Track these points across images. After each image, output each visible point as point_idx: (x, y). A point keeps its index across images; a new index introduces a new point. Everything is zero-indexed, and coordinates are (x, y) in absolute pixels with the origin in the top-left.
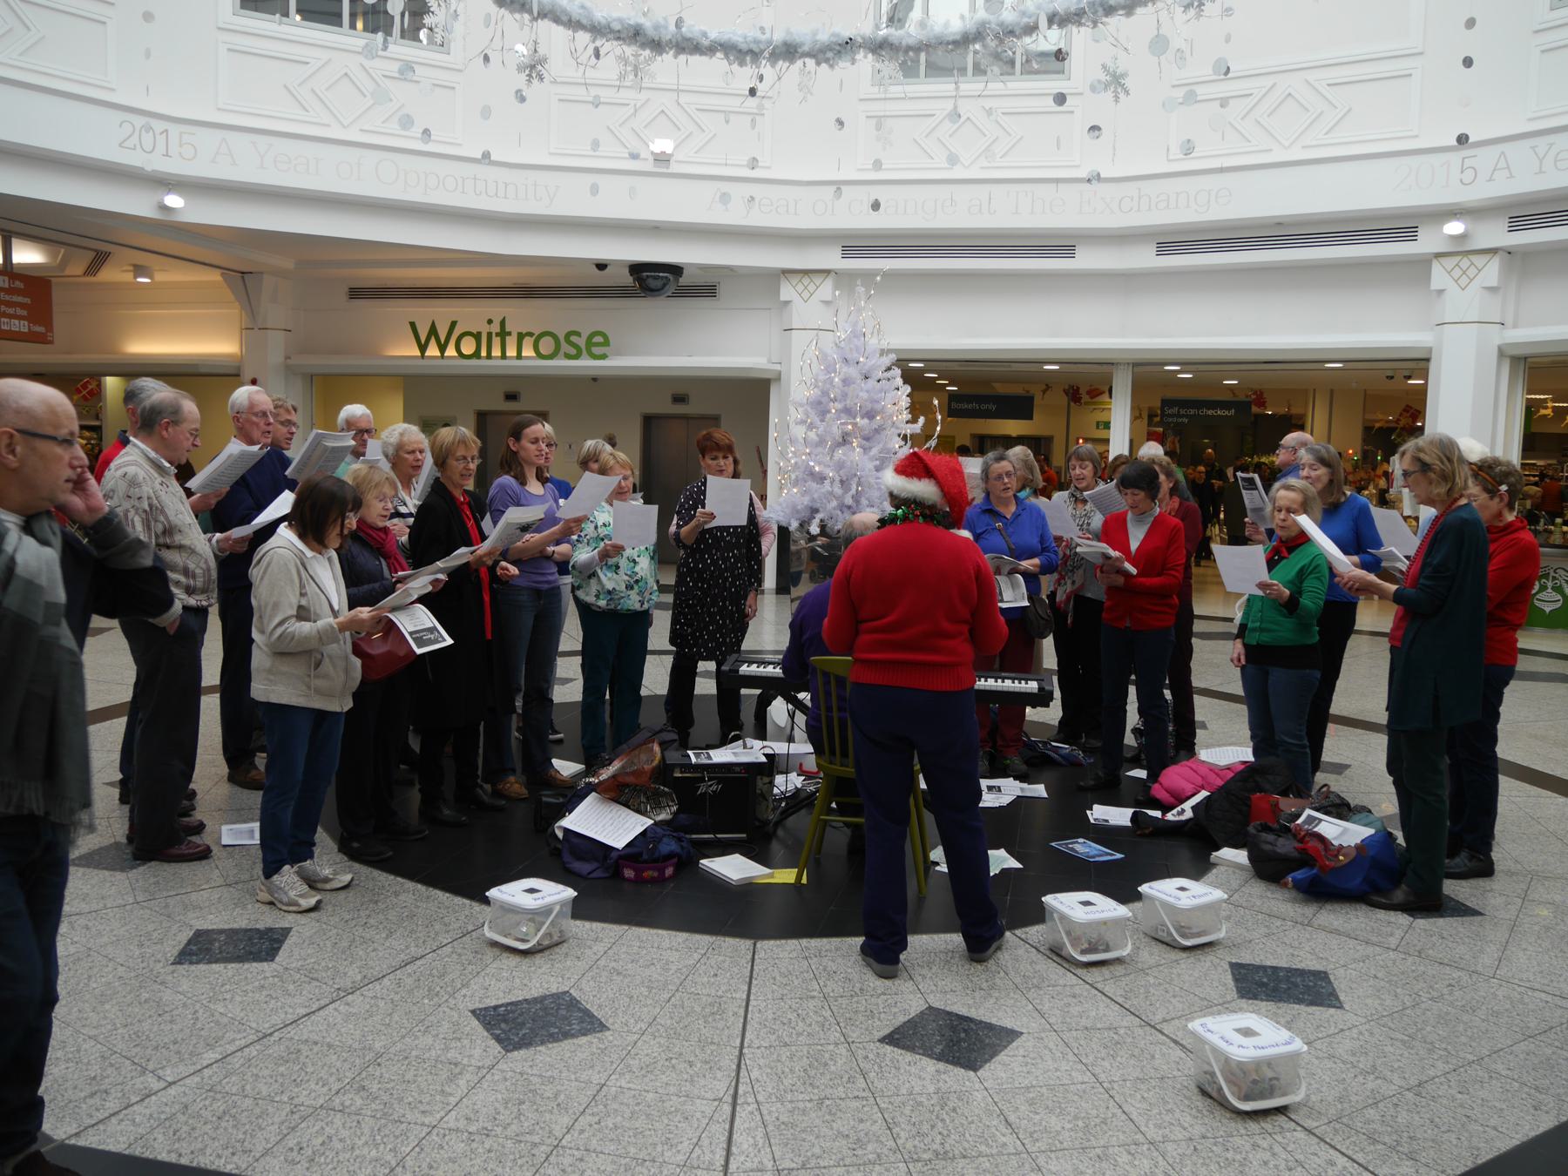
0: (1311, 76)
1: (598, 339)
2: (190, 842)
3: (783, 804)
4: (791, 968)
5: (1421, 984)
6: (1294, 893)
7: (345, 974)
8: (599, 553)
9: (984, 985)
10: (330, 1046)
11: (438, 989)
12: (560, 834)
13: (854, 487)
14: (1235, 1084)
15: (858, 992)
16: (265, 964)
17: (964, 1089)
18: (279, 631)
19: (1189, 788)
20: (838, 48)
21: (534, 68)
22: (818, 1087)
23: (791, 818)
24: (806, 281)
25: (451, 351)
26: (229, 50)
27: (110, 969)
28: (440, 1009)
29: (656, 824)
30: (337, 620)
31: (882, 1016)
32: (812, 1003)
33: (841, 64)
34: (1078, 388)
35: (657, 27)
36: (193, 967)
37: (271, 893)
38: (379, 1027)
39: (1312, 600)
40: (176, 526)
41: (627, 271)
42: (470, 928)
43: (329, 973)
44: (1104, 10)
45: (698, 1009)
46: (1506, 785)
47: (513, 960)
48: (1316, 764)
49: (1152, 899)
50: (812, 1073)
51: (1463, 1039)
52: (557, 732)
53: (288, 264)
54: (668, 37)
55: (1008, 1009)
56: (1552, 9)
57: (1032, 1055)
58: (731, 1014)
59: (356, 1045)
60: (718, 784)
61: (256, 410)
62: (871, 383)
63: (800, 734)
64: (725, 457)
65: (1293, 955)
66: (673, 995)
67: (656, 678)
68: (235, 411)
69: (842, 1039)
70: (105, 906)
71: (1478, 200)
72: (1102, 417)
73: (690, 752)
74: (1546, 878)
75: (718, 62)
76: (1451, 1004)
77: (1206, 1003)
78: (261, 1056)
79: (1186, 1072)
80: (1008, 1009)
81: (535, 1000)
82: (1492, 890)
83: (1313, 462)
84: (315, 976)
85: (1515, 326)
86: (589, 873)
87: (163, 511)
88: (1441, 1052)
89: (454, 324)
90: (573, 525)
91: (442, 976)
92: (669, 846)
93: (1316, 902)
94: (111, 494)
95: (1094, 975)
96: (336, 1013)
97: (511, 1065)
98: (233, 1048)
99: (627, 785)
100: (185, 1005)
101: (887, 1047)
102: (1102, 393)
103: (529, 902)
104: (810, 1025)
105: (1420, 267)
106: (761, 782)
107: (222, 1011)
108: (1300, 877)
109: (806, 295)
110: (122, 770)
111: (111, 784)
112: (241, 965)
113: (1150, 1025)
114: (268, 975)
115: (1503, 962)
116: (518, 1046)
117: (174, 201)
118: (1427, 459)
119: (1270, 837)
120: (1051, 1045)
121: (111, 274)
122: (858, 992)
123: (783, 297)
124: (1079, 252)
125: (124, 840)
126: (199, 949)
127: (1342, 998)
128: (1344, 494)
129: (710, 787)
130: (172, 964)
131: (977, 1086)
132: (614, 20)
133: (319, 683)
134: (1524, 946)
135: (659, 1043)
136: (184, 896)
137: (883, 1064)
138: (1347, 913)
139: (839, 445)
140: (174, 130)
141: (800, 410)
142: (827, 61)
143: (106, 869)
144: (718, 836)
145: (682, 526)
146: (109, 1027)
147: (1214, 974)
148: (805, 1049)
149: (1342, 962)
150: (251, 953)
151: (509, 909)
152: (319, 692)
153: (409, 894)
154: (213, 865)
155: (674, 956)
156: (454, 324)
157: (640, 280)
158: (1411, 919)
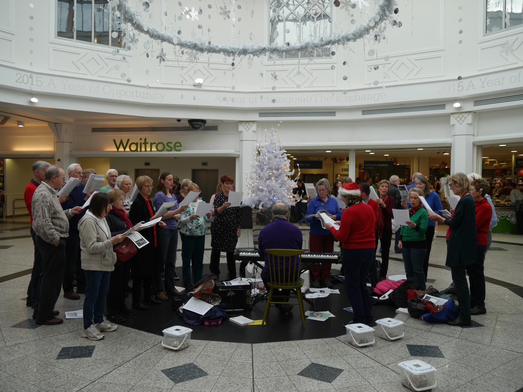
0: (409, 57)
1: (178, 145)
2: (56, 318)
3: (254, 299)
4: (265, 352)
5: (468, 349)
6: (424, 322)
7: (117, 360)
8: (190, 218)
9: (329, 355)
10: (116, 384)
11: (149, 364)
12: (181, 312)
14: (415, 383)
15: (288, 359)
16: (88, 358)
17: (328, 389)
18: (92, 246)
19: (386, 289)
20: (260, 51)
21: (161, 58)
22: (280, 390)
23: (257, 304)
24: (247, 124)
25: (128, 149)
26: (53, 50)
27: (35, 362)
28: (151, 370)
29: (214, 306)
31: (297, 366)
32: (274, 363)
33: (261, 56)
34: (336, 158)
35: (202, 44)
36: (64, 360)
37: (87, 334)
38: (131, 377)
39: (424, 226)
40: (57, 211)
41: (187, 122)
42: (156, 343)
43: (111, 360)
44: (347, 39)
45: (237, 367)
46: (487, 284)
47: (173, 353)
48: (426, 280)
49: (380, 325)
50: (278, 386)
51: (483, 366)
52: (177, 277)
53: (71, 120)
54: (206, 47)
55: (338, 363)
56: (484, 36)
57: (348, 377)
58: (248, 368)
59: (124, 384)
60: (234, 293)
61: (77, 171)
62: (277, 159)
63: (258, 275)
64: (231, 184)
65: (426, 341)
66: (228, 363)
67: (207, 259)
68: (70, 171)
69: (286, 375)
70: (29, 340)
71: (463, 96)
72: (345, 167)
73: (224, 282)
74: (502, 313)
75: (221, 55)
76: (478, 355)
77: (401, 358)
78: (93, 388)
79: (398, 380)
80: (338, 363)
81: (182, 366)
82: (486, 318)
83: (420, 182)
84: (106, 361)
85: (478, 136)
86: (193, 324)
87: (53, 206)
88: (477, 370)
89: (128, 140)
90: (184, 208)
91: (149, 359)
92: (219, 314)
93: (432, 324)
94: (37, 201)
95: (364, 350)
96: (116, 373)
97: (178, 388)
98: (83, 386)
99: (204, 294)
100: (63, 373)
101: (301, 376)
102: (344, 159)
103: (177, 333)
104: (274, 370)
105: (446, 118)
107: (77, 374)
108: (426, 316)
109: (247, 129)
110: (28, 294)
111: (23, 299)
112: (80, 358)
113: (384, 366)
114: (90, 361)
115: (493, 341)
116: (179, 382)
117: (34, 100)
118: (455, 180)
119: (415, 304)
120: (353, 373)
121: (8, 124)
122: (288, 359)
124: (337, 114)
125: (32, 318)
126: (65, 354)
127: (444, 354)
128: (430, 192)
129: (231, 294)
130: (56, 359)
131: (332, 387)
132: (188, 42)
133: (105, 262)
134: (498, 335)
135: (226, 378)
136: (56, 336)
137: (300, 382)
138: (441, 327)
139: (268, 179)
140: (34, 76)
141: (254, 168)
142: (257, 55)
143: (27, 328)
144: (235, 310)
145: (217, 208)
146: (38, 381)
147: (401, 349)
148: (274, 378)
149: (442, 343)
150: (83, 354)
151: (170, 336)
152: (105, 265)
153: (133, 333)
154: (64, 325)
155: (226, 350)
156: (128, 140)
157: (192, 125)
158: (462, 328)
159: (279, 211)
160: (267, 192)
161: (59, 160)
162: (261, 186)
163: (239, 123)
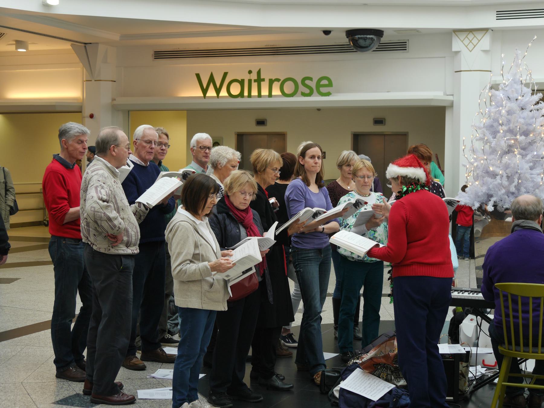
1: (325, 82)
3: (474, 383)
12: (337, 395)
13: (516, 180)
18: (179, 268)
24: (471, 36)
25: (224, 93)
30: (209, 263)
41: (344, 35)
53: (115, 37)
61: (146, 139)
62: (526, 113)
89: (225, 74)
99: (379, 364)
106: (462, 366)
109: (471, 46)
123: (455, 48)
156: (225, 74)
159: (525, 213)
160: (505, 178)
161: (92, 116)
162: (493, 165)
163: (453, 33)
